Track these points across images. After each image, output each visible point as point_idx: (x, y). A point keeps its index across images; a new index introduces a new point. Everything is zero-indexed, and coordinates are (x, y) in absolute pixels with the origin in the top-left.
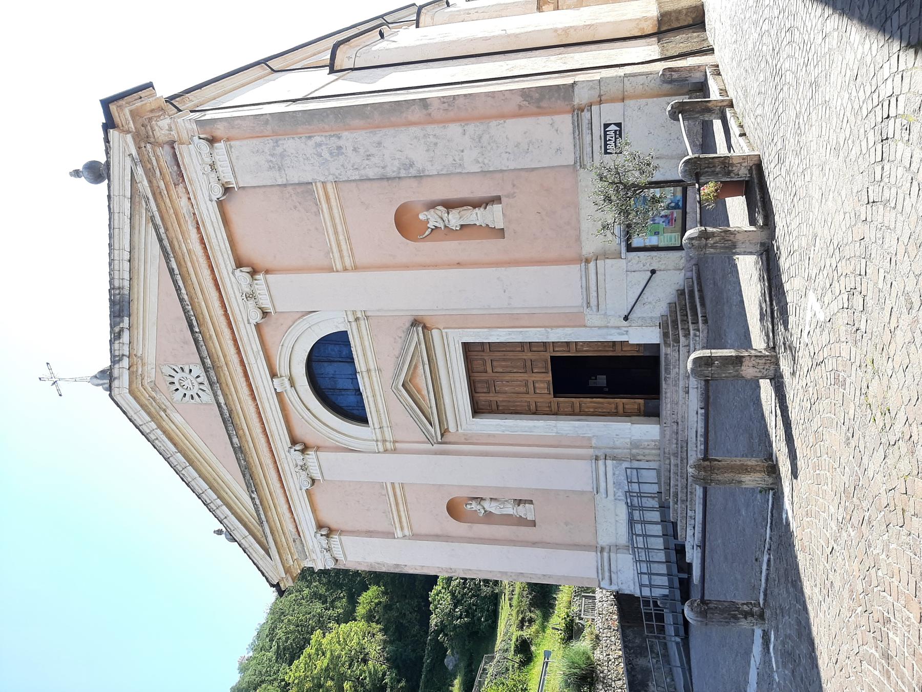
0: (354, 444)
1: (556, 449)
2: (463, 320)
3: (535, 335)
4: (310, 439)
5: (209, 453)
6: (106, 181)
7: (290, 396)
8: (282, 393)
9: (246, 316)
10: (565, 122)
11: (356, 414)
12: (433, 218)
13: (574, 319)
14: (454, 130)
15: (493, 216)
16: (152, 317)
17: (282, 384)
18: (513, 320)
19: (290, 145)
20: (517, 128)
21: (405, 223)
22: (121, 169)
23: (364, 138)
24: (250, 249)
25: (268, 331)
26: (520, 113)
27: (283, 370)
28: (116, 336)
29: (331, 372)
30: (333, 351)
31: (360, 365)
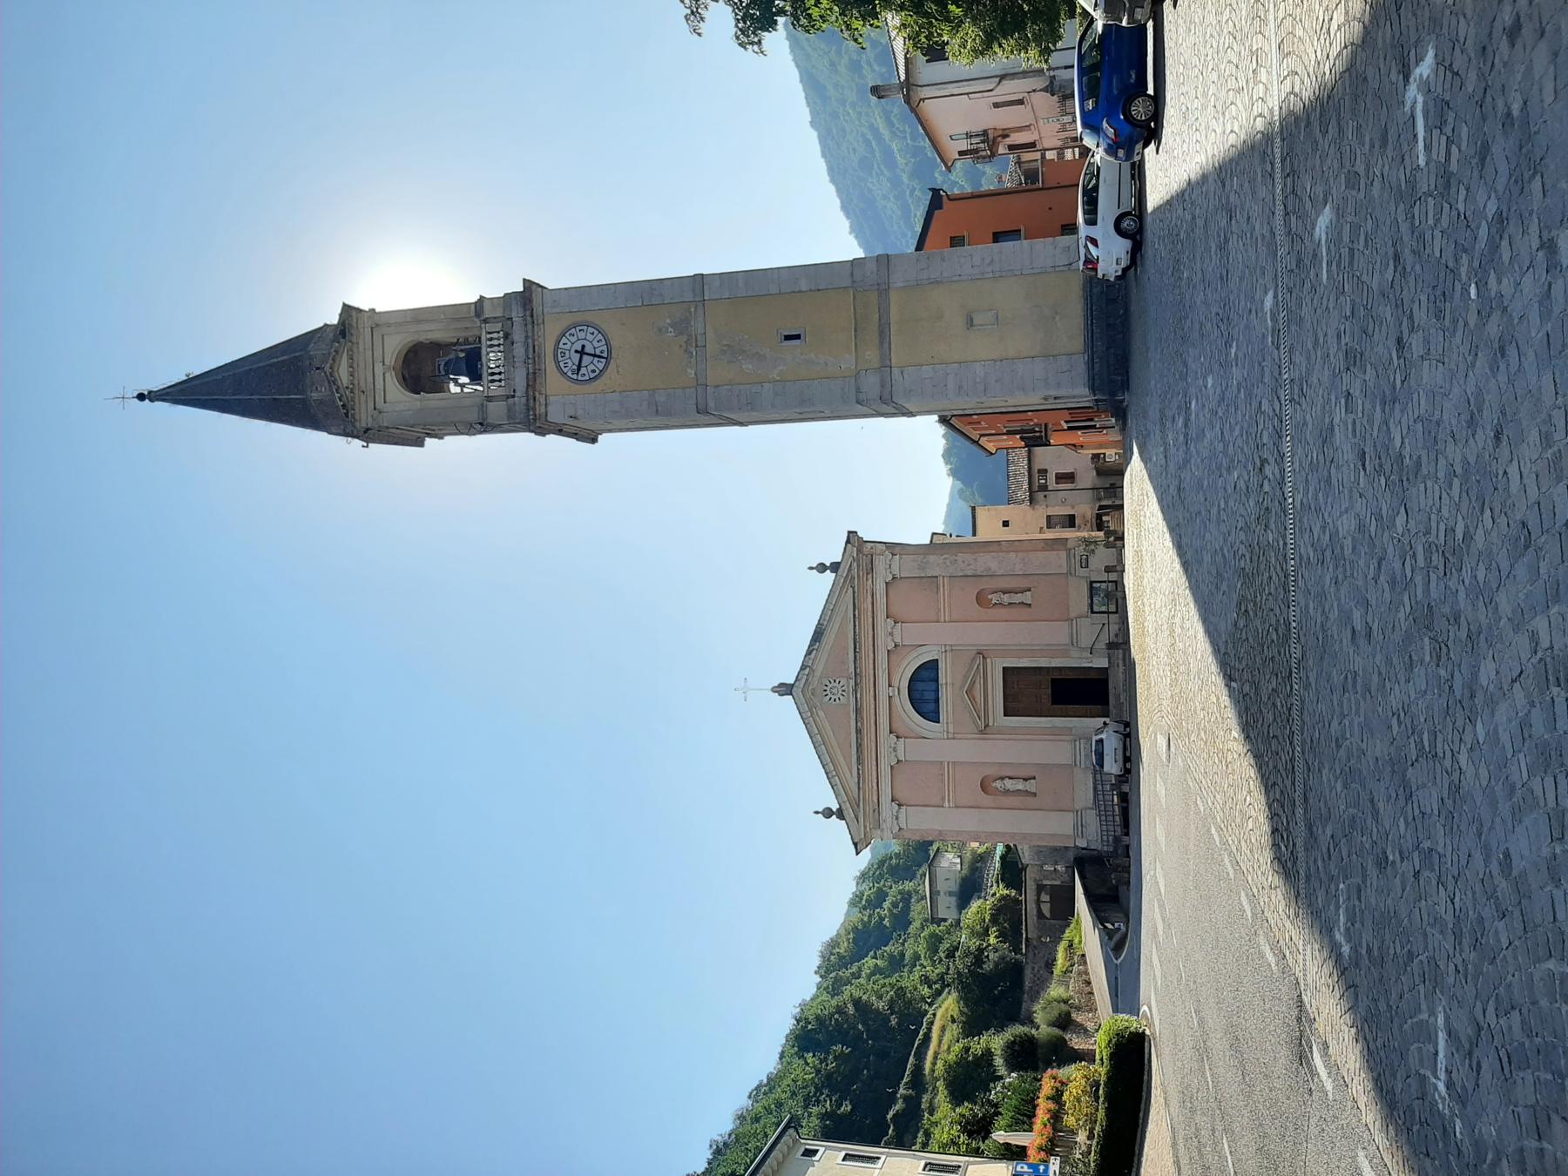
0: (926, 733)
1: (1054, 732)
2: (1005, 652)
3: (1043, 662)
4: (900, 732)
5: (834, 743)
6: (1153, 199)
7: (896, 700)
8: (894, 689)
9: (884, 643)
10: (1063, 554)
11: (933, 716)
12: (994, 598)
13: (1065, 653)
14: (1012, 555)
15: (1027, 598)
16: (828, 647)
17: (893, 692)
18: (1031, 653)
19: (932, 558)
20: (1042, 555)
21: (981, 599)
22: (843, 570)
23: (969, 557)
24: (894, 610)
25: (893, 658)
26: (1043, 550)
27: (895, 683)
28: (809, 653)
29: (924, 690)
30: (925, 674)
31: (942, 680)
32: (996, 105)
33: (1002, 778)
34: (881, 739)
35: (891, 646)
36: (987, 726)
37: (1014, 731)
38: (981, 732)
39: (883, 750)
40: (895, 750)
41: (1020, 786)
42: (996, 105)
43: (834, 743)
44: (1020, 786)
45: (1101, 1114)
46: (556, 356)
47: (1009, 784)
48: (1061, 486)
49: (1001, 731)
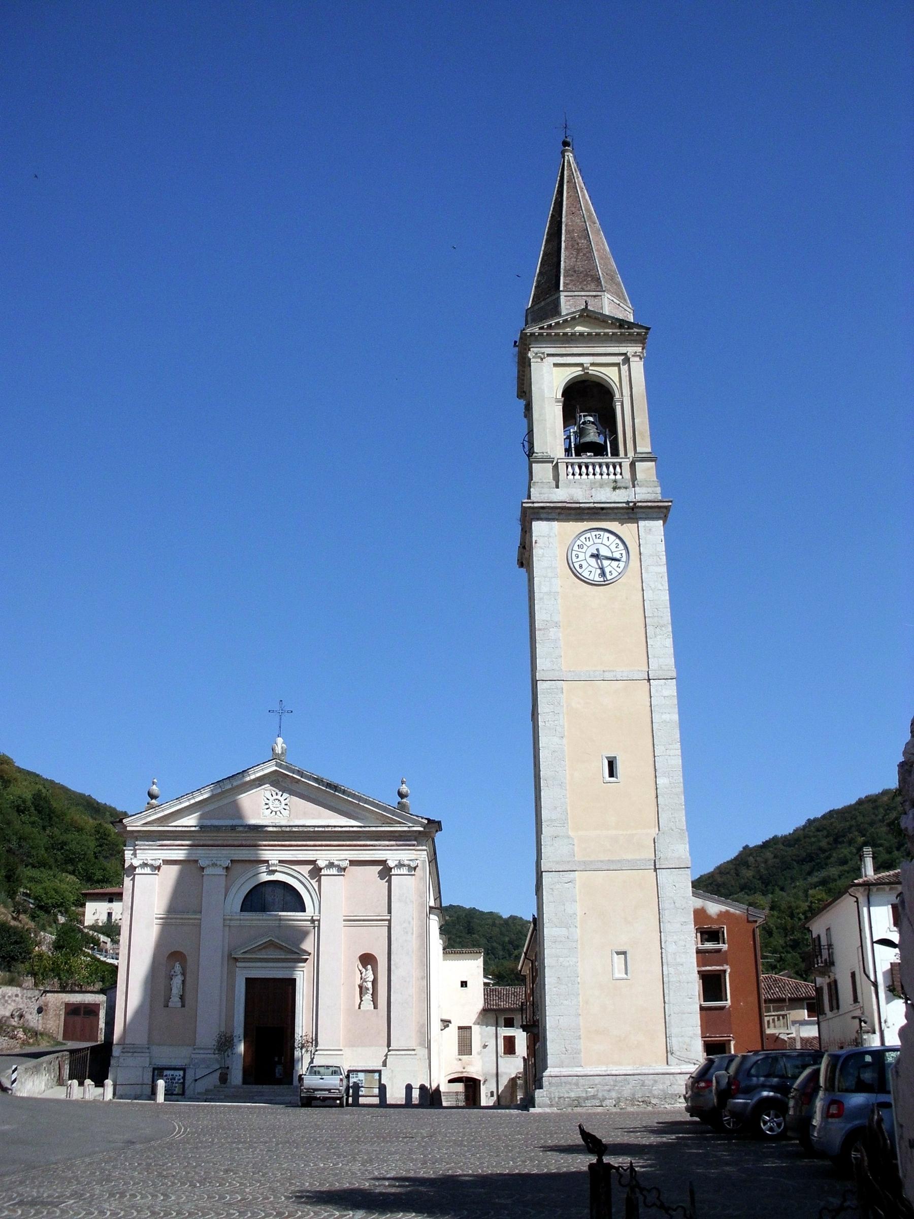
5: (221, 803)
32: (853, 975)
33: (184, 974)
34: (226, 851)
35: (202, 863)
36: (236, 960)
37: (231, 988)
38: (230, 955)
39: (214, 852)
40: (214, 865)
41: (176, 990)
42: (853, 975)
43: (221, 803)
44: (176, 990)
45: (467, 1178)
46: (598, 529)
47: (177, 981)
48: (501, 1042)
49: (231, 975)
